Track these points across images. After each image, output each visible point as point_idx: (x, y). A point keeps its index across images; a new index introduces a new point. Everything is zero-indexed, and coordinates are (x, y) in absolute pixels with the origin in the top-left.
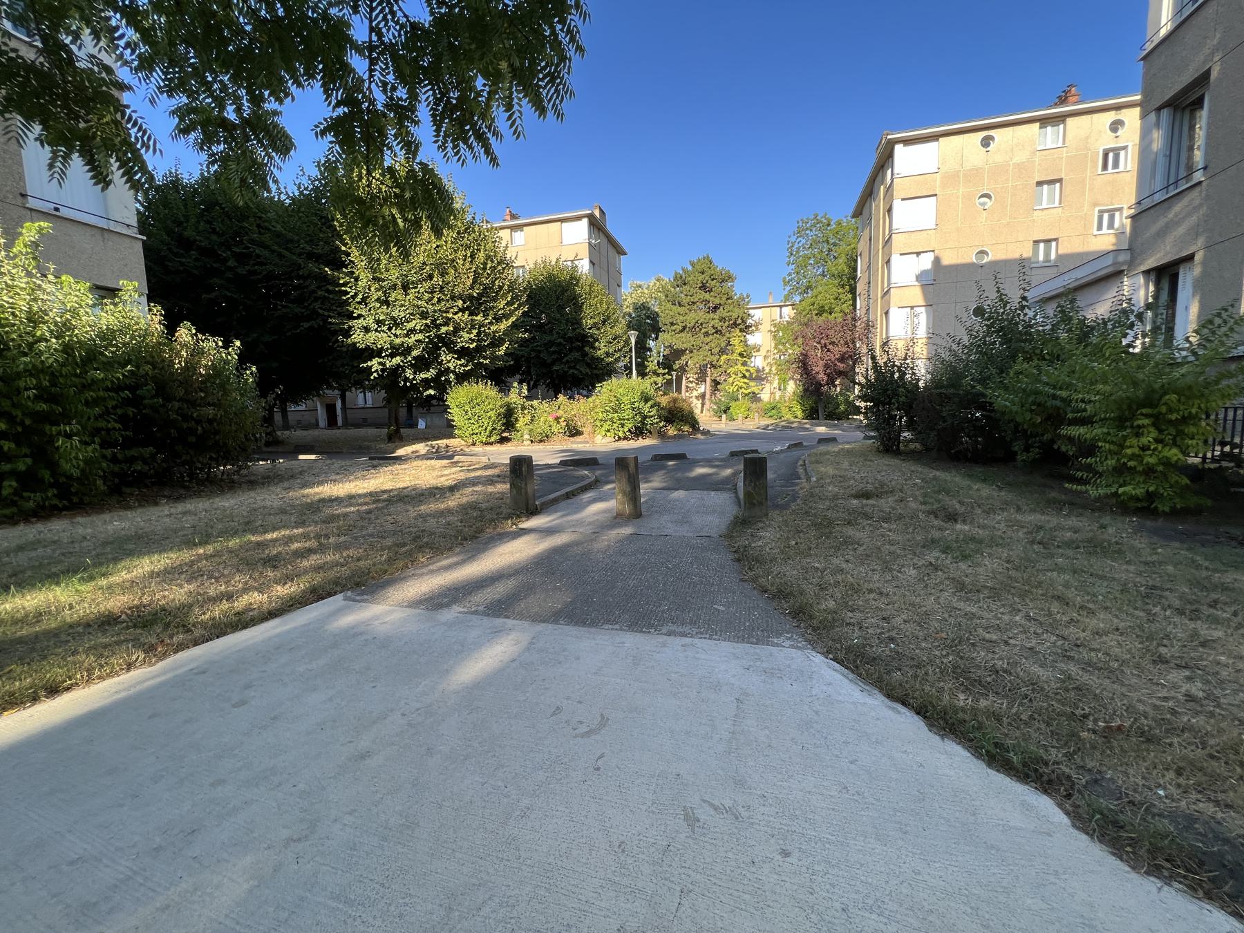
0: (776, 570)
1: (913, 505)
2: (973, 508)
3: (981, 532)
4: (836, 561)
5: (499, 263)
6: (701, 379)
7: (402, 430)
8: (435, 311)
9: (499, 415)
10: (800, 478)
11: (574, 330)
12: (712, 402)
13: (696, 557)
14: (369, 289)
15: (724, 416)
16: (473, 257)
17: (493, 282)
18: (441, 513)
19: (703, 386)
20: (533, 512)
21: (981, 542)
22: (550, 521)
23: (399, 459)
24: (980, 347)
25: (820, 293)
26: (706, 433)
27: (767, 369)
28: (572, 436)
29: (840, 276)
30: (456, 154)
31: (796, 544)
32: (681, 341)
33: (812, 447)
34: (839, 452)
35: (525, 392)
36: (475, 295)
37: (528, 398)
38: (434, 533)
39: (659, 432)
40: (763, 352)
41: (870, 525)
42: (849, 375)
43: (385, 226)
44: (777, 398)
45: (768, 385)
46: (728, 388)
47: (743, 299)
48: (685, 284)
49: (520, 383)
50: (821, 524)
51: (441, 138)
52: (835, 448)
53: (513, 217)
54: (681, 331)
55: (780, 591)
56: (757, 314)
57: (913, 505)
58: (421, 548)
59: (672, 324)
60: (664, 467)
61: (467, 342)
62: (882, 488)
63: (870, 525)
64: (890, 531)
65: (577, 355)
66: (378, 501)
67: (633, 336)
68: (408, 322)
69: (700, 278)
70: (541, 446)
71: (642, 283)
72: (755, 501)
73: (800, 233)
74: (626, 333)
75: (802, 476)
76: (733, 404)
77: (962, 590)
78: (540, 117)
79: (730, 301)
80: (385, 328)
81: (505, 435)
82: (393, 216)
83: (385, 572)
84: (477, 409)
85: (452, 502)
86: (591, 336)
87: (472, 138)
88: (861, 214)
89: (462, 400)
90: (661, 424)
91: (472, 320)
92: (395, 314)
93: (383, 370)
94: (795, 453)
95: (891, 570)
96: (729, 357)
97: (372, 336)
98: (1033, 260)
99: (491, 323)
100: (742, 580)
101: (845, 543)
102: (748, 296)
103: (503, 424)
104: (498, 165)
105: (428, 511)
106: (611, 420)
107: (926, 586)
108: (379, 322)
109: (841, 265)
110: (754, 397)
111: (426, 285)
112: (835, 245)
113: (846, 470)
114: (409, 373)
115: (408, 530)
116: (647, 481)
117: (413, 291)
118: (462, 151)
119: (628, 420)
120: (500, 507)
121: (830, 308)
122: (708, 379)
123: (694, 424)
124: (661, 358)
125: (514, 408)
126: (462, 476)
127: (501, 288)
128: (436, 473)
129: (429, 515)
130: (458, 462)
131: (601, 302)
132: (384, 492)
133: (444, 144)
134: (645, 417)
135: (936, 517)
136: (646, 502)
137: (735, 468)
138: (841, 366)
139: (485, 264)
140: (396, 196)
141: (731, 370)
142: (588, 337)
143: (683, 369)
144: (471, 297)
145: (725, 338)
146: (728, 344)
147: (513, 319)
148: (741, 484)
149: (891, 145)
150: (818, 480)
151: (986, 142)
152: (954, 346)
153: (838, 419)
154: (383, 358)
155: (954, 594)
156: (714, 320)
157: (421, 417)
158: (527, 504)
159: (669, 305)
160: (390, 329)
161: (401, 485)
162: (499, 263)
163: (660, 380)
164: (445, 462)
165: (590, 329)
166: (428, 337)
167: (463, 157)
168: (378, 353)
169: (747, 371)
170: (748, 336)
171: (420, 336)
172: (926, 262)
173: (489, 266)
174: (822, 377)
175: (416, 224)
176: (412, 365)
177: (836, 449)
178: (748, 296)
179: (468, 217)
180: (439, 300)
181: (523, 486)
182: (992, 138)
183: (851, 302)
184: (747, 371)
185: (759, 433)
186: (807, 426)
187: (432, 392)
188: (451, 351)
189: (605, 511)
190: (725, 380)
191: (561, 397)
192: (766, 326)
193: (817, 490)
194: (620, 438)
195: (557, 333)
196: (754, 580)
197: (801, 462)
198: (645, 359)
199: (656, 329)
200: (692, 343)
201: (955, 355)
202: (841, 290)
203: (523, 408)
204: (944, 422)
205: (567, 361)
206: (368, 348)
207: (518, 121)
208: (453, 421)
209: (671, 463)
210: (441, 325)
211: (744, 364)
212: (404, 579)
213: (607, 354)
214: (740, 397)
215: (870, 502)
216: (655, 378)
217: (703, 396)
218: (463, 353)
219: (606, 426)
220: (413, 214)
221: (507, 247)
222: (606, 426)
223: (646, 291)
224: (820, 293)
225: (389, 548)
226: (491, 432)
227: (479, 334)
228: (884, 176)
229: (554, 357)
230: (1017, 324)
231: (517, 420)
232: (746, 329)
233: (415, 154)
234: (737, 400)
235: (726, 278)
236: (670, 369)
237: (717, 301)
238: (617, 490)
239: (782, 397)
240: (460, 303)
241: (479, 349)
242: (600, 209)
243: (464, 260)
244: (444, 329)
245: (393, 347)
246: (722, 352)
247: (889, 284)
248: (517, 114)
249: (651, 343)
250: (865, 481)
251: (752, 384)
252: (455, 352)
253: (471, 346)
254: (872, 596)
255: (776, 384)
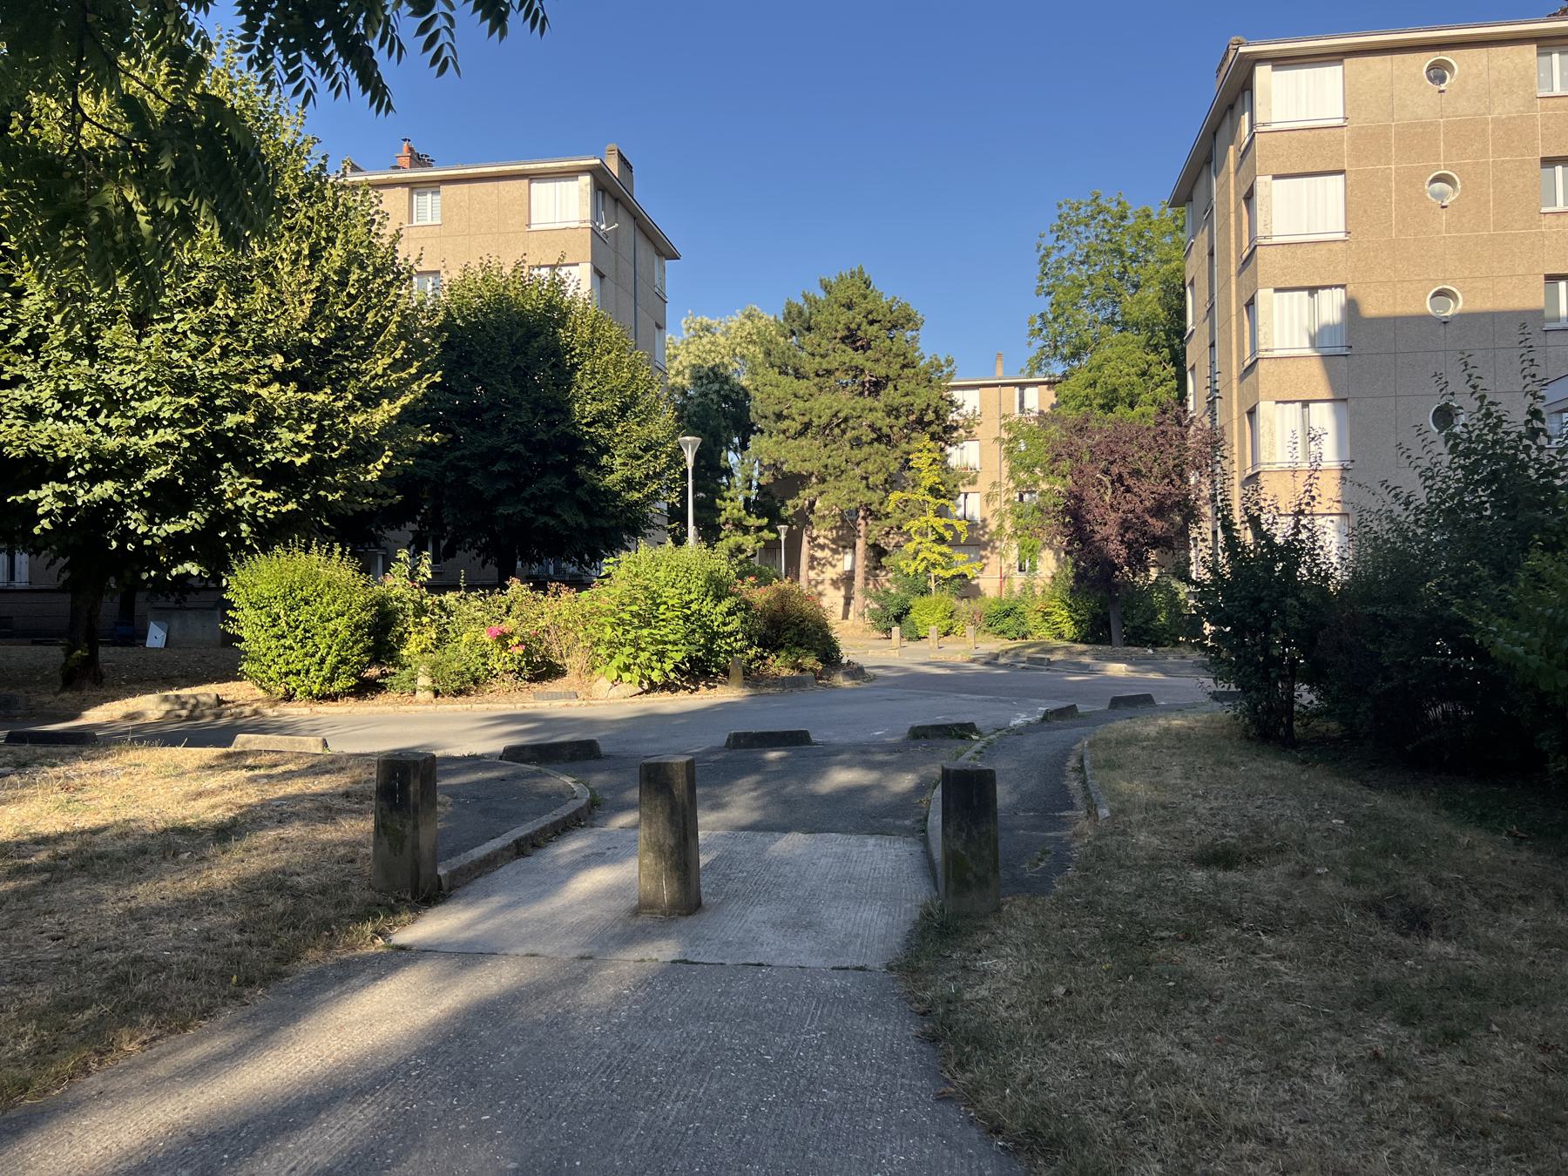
0: (1022, 1067)
1: (1328, 886)
2: (1461, 895)
3: (1482, 961)
4: (1161, 1045)
5: (377, 272)
6: (845, 542)
7: (104, 653)
8: (212, 378)
9: (358, 627)
10: (1071, 806)
11: (552, 424)
12: (867, 595)
13: (831, 1031)
14: (48, 318)
15: (896, 630)
16: (315, 255)
17: (362, 317)
18: (191, 907)
19: (848, 558)
20: (429, 895)
21: (1480, 994)
22: (469, 925)
23: (86, 742)
24: (1449, 514)
25: (1108, 360)
26: (856, 672)
27: (993, 525)
28: (537, 678)
29: (1149, 325)
30: (292, 78)
31: (1068, 992)
32: (798, 456)
33: (1092, 719)
34: (1159, 738)
35: (426, 570)
36: (315, 342)
37: (435, 587)
38: (164, 967)
39: (747, 673)
40: (984, 484)
41: (1234, 940)
42: (1175, 543)
43: (107, 223)
44: (1017, 589)
45: (994, 560)
46: (904, 562)
47: (939, 368)
48: (809, 329)
49: (418, 547)
50: (1123, 937)
51: (257, 42)
52: (1150, 726)
53: (418, 160)
54: (801, 433)
55: (1033, 1133)
56: (970, 401)
57: (1328, 886)
58: (127, 1015)
59: (779, 417)
60: (758, 767)
61: (287, 450)
62: (1260, 839)
63: (1234, 940)
64: (1281, 958)
65: (556, 482)
66: (23, 871)
67: (690, 447)
68: (141, 399)
69: (843, 319)
70: (460, 706)
71: (714, 323)
72: (970, 876)
73: (1060, 233)
74: (674, 438)
75: (1078, 801)
76: (917, 602)
77: (1450, 1131)
78: (492, 32)
79: (908, 372)
80: (81, 413)
81: (374, 672)
82: (128, 206)
83: (25, 1086)
84: (303, 614)
85: (223, 872)
86: (593, 442)
87: (332, 46)
88: (1190, 199)
89: (264, 589)
90: (751, 653)
91: (303, 403)
92: (112, 377)
93: (67, 513)
94: (1061, 734)
95: (1287, 1073)
96: (906, 495)
97: (46, 430)
98: (1547, 314)
99: (351, 408)
100: (942, 1098)
101: (1179, 992)
102: (949, 362)
103: (367, 650)
104: (389, 107)
105: (154, 901)
106: (635, 643)
107: (1369, 1121)
108: (67, 398)
109: (1148, 305)
110: (965, 588)
111: (195, 316)
112: (1134, 259)
113: (1175, 789)
114: (136, 520)
115: (96, 956)
116: (717, 806)
117: (160, 327)
118: (306, 72)
119: (675, 643)
120: (345, 885)
121: (1131, 394)
122: (860, 544)
123: (829, 654)
124: (754, 491)
125: (397, 611)
126: (251, 796)
127: (380, 328)
128: (187, 785)
129: (157, 912)
130: (242, 754)
131: (617, 364)
132: (42, 841)
133: (262, 54)
134: (714, 636)
135: (1382, 916)
136: (711, 867)
137: (923, 771)
138: (1157, 526)
139: (344, 272)
140: (139, 158)
141: (912, 525)
142: (580, 441)
143: (804, 518)
144: (304, 348)
145: (898, 453)
146: (906, 465)
147: (405, 400)
148: (935, 819)
149: (1249, 64)
150: (1116, 813)
151: (1438, 73)
152: (1398, 509)
153: (1156, 644)
154: (70, 482)
155: (1431, 1139)
156: (874, 411)
157: (156, 619)
158: (416, 875)
159: (773, 375)
160: (94, 413)
161: (87, 821)
162: (377, 272)
163: (749, 542)
164: (210, 753)
165: (589, 425)
166: (190, 437)
167: (308, 86)
168: (59, 470)
169: (948, 527)
170: (949, 450)
171: (167, 435)
172: (1330, 306)
173: (353, 277)
174: (1116, 550)
175: (185, 224)
176: (143, 503)
177: (1152, 730)
178: (949, 362)
179: (310, 166)
180: (225, 352)
181: (408, 830)
182: (1447, 66)
183: (1174, 383)
184: (948, 527)
185: (978, 675)
186: (1086, 660)
187: (193, 568)
188: (245, 470)
189: (613, 892)
190: (898, 546)
191: (516, 586)
192: (990, 429)
193: (1112, 842)
194: (653, 687)
195: (511, 431)
196: (972, 1095)
197: (1072, 762)
198: (716, 493)
199: (746, 429)
200: (825, 460)
201: (1401, 532)
202: (1152, 357)
203: (421, 611)
204: (1387, 679)
205: (533, 497)
206: (31, 456)
207: (444, 37)
208: (241, 639)
209: (773, 755)
210: (225, 409)
211: (941, 512)
212: (73, 1107)
213: (630, 484)
214: (932, 585)
215: (1233, 876)
216: (738, 538)
217: (848, 579)
218: (277, 476)
219: (620, 659)
220: (178, 204)
221: (397, 236)
222: (620, 659)
223: (722, 340)
224: (1108, 360)
225: (41, 1016)
226: (335, 669)
227: (317, 435)
228: (1235, 127)
229: (502, 486)
230: (1525, 467)
231: (401, 639)
232: (945, 433)
233: (194, 78)
234: (925, 592)
235: (901, 321)
236: (774, 517)
237: (881, 370)
238: (643, 833)
239: (1028, 588)
240: (278, 361)
241: (314, 468)
242: (621, 157)
243: (294, 262)
244: (231, 420)
245: (96, 455)
246: (891, 483)
247: (1254, 352)
248: (441, 22)
249: (732, 458)
250: (1218, 820)
251: (959, 557)
252: (257, 474)
253: (298, 462)
254: (1249, 1147)
255: (1013, 556)
